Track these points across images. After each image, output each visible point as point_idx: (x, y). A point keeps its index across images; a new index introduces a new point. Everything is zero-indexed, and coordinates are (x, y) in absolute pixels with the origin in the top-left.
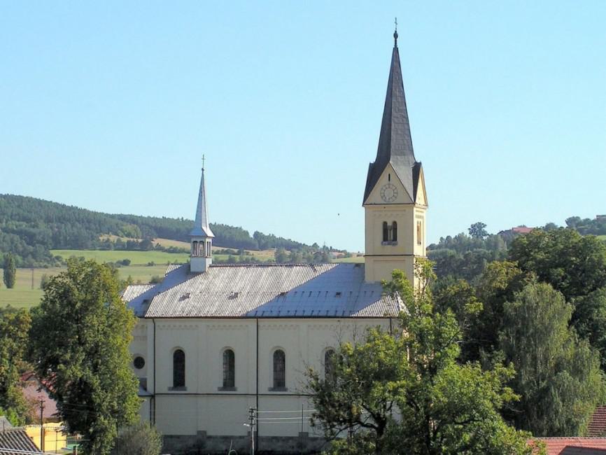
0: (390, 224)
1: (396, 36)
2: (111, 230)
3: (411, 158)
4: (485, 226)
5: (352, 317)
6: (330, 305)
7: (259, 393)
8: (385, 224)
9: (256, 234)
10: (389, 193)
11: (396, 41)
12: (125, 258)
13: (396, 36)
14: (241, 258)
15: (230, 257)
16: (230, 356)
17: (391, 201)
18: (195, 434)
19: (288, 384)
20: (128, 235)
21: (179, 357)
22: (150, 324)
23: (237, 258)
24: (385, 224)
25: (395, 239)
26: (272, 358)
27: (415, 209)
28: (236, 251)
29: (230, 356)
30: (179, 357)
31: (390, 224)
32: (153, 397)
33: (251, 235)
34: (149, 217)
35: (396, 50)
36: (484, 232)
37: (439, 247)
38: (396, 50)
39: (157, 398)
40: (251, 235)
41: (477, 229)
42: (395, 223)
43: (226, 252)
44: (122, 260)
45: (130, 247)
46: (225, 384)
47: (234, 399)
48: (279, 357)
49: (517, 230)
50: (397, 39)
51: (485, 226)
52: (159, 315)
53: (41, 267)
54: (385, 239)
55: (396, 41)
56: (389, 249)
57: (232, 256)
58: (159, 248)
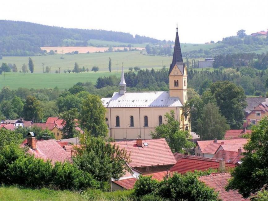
0: (176, 81)
1: (177, 29)
2: (69, 37)
3: (182, 63)
4: (245, 31)
5: (184, 68)
6: (161, 104)
7: (141, 127)
8: (175, 81)
9: (137, 36)
10: (176, 73)
11: (177, 31)
12: (74, 51)
13: (177, 29)
14: (130, 49)
15: (124, 48)
16: (132, 118)
17: (177, 75)
18: (123, 139)
19: (134, 125)
20: (77, 39)
21: (118, 118)
22: (109, 109)
23: (128, 49)
24: (175, 81)
25: (178, 85)
26: (144, 118)
27: (183, 78)
28: (127, 44)
29: (132, 118)
30: (118, 118)
31: (176, 81)
32: (111, 129)
33: (134, 36)
34: (85, 30)
35: (177, 33)
36: (244, 34)
37: (222, 42)
38: (177, 33)
39: (112, 129)
40: (134, 36)
41: (241, 33)
42: (178, 81)
43: (123, 46)
44: (74, 51)
45: (78, 45)
46: (131, 126)
47: (134, 129)
48: (146, 118)
49: (260, 33)
50: (176, 31)
51: (245, 31)
52: (112, 107)
53: (37, 56)
54: (175, 85)
55: (177, 31)
56: (176, 88)
57: (126, 48)
58: (92, 45)
